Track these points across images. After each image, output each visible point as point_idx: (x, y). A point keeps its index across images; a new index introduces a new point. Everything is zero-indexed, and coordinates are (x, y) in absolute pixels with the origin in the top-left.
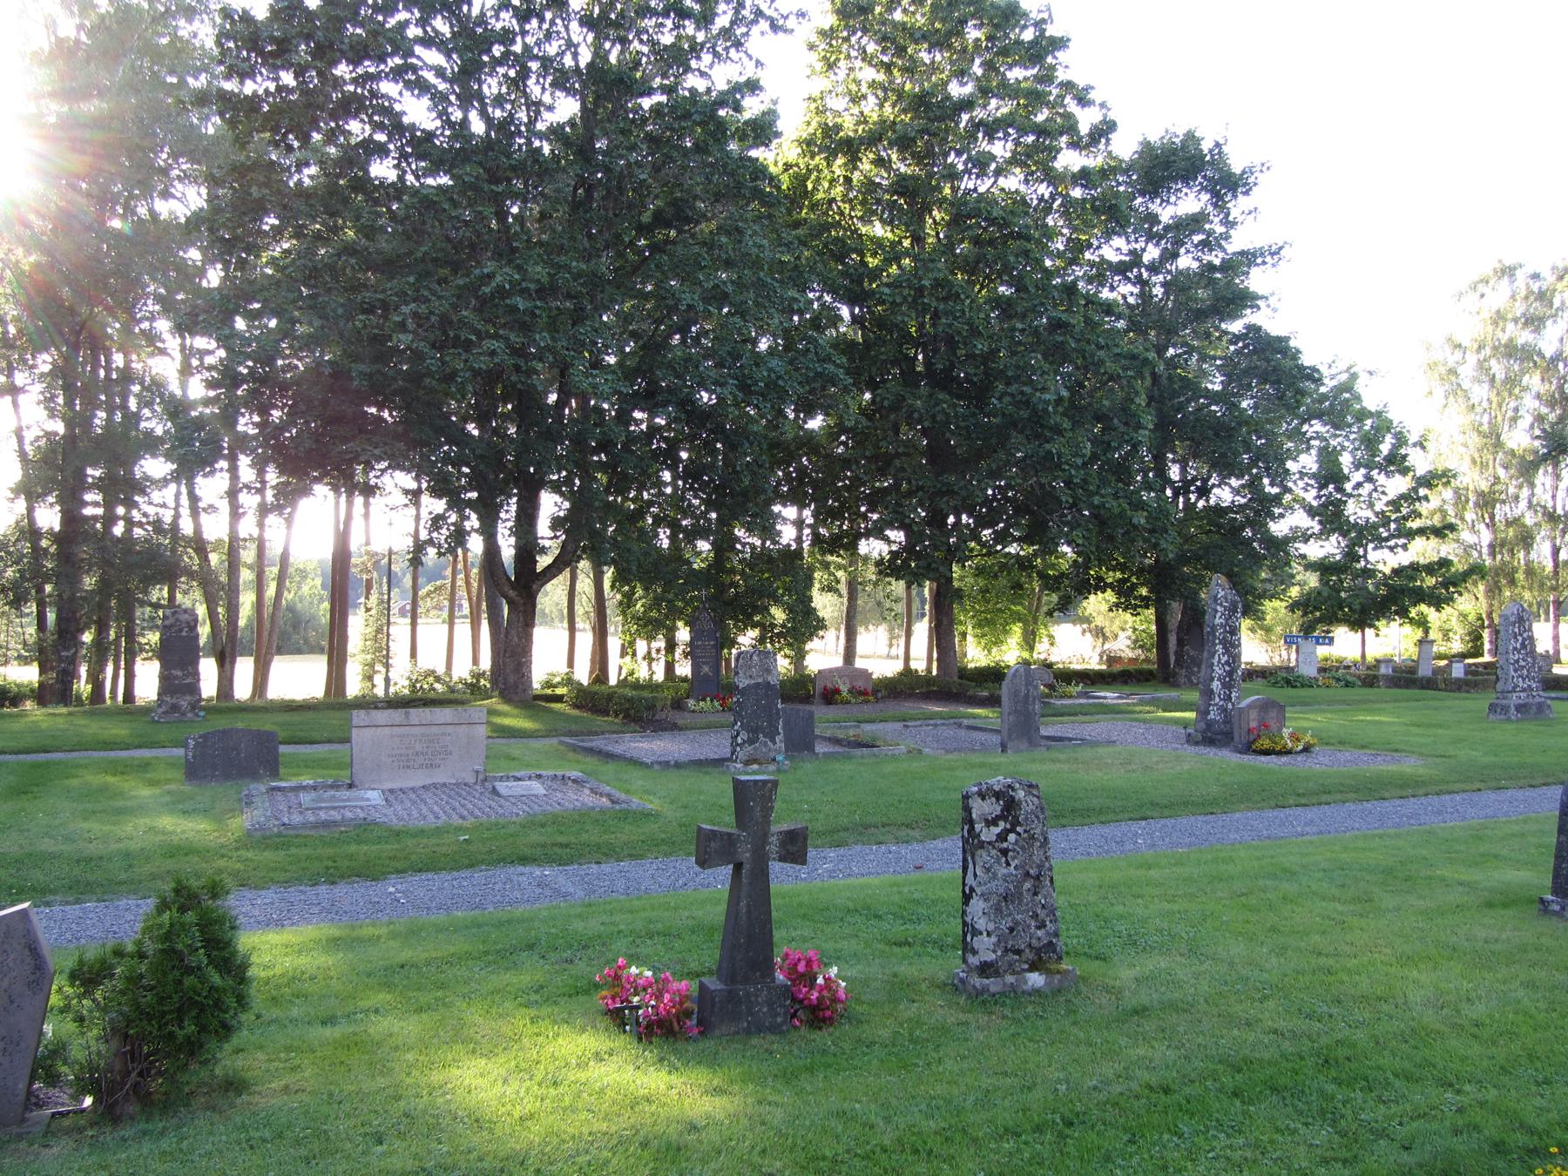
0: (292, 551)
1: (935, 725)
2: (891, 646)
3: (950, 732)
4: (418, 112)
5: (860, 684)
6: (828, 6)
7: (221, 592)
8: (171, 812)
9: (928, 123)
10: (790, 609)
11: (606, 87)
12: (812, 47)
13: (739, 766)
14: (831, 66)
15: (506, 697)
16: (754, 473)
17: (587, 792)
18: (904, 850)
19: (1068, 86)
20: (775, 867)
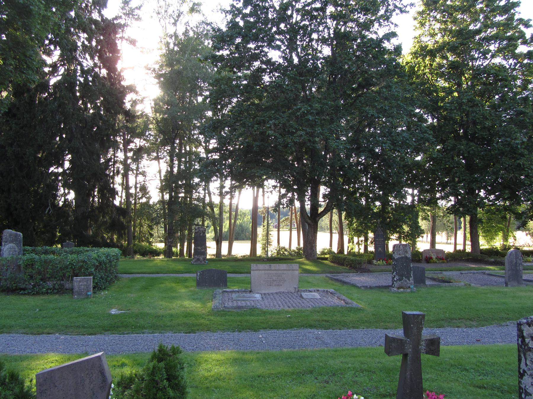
0: (240, 207)
1: (474, 273)
2: (448, 239)
3: (480, 276)
4: (275, 56)
5: (440, 255)
6: (421, 3)
7: (217, 222)
8: (189, 299)
9: (462, 42)
10: (409, 226)
11: (341, 40)
12: (415, 19)
13: (395, 289)
14: (422, 25)
15: (307, 258)
16: (398, 176)
17: (336, 298)
18: (470, 331)
19: (521, 20)
20: (425, 357)
